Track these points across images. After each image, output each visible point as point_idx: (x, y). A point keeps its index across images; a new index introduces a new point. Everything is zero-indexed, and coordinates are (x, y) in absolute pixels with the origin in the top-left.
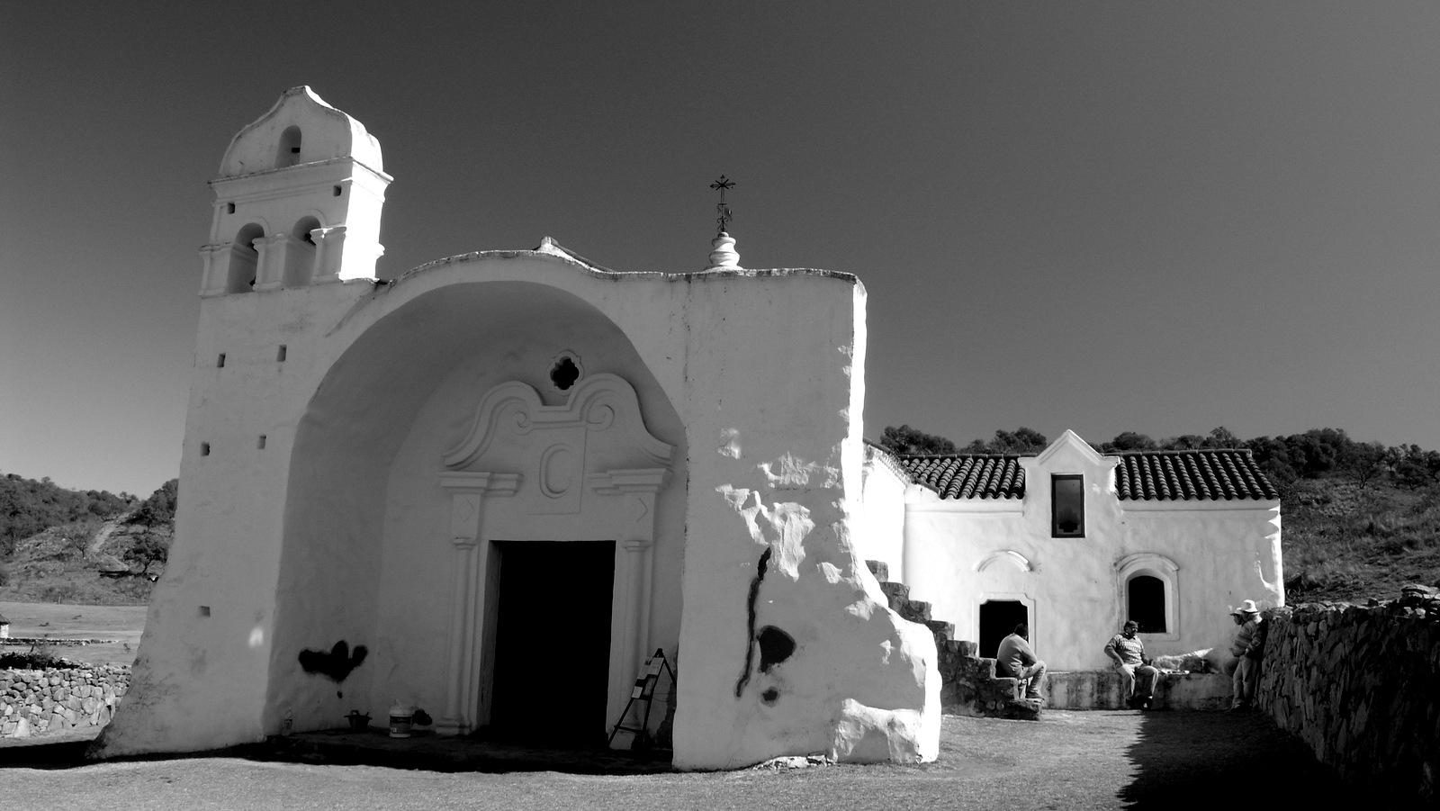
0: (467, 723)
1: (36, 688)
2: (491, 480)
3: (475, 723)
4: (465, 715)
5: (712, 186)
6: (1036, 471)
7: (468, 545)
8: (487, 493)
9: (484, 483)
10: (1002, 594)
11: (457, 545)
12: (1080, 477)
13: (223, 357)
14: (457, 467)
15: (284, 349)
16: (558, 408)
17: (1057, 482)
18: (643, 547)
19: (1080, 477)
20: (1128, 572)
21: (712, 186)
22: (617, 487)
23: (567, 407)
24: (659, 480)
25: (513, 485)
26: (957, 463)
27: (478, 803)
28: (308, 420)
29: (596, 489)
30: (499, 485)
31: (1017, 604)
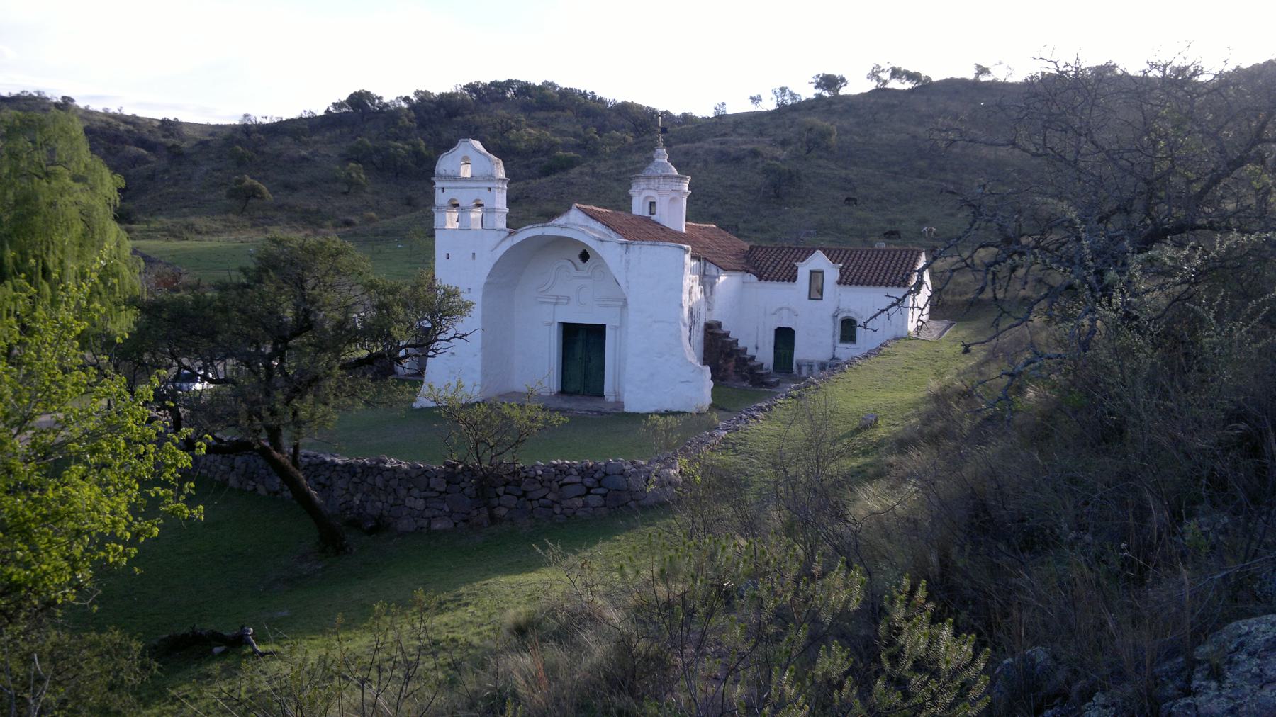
6: (804, 270)
7: (550, 324)
8: (556, 303)
9: (554, 301)
18: (616, 328)
20: (840, 317)
28: (487, 283)
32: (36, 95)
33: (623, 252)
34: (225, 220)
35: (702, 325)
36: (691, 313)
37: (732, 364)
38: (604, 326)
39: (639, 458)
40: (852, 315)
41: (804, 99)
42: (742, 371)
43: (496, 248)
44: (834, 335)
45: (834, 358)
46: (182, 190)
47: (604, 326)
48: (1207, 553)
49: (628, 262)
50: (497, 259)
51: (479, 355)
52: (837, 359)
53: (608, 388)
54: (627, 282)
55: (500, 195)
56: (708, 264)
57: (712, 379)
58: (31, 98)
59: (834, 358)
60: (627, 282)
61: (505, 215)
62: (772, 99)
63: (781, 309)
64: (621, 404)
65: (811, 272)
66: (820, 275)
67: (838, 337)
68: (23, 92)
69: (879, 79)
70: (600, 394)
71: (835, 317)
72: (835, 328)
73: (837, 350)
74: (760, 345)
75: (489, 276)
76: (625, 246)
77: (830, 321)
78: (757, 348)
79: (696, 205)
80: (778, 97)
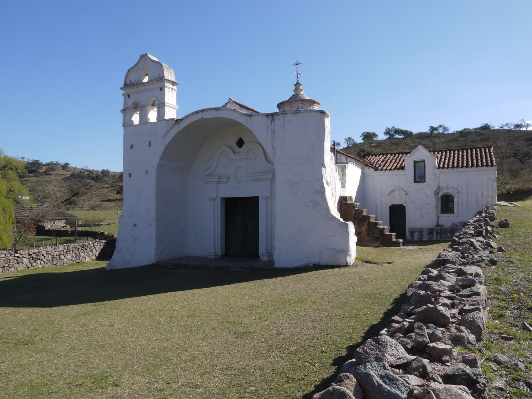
0: (218, 254)
1: (90, 247)
2: (219, 178)
3: (220, 254)
4: (217, 252)
5: (293, 65)
7: (214, 200)
8: (218, 182)
9: (217, 180)
10: (397, 202)
11: (211, 199)
12: (424, 161)
13: (132, 146)
14: (208, 175)
15: (150, 142)
16: (240, 155)
17: (416, 163)
18: (267, 198)
19: (424, 161)
20: (440, 194)
21: (293, 65)
22: (258, 179)
23: (241, 154)
24: (271, 177)
25: (226, 180)
26: (385, 156)
27: (4, 325)
28: (160, 165)
29: (252, 180)
30: (222, 180)
31: (402, 205)
32: (56, 163)
33: (269, 123)
38: (257, 198)
40: (450, 191)
41: (358, 143)
42: (373, 233)
43: (166, 134)
44: (437, 208)
45: (438, 225)
47: (257, 198)
48: (69, 251)
49: (273, 131)
50: (167, 144)
51: (154, 224)
52: (441, 226)
53: (262, 249)
54: (273, 148)
56: (338, 155)
57: (355, 234)
58: (54, 164)
59: (438, 225)
60: (273, 148)
62: (345, 143)
63: (393, 191)
64: (273, 262)
65: (415, 162)
67: (439, 210)
68: (51, 162)
69: (390, 134)
70: (256, 255)
71: (436, 193)
72: (437, 203)
73: (440, 219)
75: (162, 158)
76: (270, 117)
77: (433, 197)
80: (347, 142)
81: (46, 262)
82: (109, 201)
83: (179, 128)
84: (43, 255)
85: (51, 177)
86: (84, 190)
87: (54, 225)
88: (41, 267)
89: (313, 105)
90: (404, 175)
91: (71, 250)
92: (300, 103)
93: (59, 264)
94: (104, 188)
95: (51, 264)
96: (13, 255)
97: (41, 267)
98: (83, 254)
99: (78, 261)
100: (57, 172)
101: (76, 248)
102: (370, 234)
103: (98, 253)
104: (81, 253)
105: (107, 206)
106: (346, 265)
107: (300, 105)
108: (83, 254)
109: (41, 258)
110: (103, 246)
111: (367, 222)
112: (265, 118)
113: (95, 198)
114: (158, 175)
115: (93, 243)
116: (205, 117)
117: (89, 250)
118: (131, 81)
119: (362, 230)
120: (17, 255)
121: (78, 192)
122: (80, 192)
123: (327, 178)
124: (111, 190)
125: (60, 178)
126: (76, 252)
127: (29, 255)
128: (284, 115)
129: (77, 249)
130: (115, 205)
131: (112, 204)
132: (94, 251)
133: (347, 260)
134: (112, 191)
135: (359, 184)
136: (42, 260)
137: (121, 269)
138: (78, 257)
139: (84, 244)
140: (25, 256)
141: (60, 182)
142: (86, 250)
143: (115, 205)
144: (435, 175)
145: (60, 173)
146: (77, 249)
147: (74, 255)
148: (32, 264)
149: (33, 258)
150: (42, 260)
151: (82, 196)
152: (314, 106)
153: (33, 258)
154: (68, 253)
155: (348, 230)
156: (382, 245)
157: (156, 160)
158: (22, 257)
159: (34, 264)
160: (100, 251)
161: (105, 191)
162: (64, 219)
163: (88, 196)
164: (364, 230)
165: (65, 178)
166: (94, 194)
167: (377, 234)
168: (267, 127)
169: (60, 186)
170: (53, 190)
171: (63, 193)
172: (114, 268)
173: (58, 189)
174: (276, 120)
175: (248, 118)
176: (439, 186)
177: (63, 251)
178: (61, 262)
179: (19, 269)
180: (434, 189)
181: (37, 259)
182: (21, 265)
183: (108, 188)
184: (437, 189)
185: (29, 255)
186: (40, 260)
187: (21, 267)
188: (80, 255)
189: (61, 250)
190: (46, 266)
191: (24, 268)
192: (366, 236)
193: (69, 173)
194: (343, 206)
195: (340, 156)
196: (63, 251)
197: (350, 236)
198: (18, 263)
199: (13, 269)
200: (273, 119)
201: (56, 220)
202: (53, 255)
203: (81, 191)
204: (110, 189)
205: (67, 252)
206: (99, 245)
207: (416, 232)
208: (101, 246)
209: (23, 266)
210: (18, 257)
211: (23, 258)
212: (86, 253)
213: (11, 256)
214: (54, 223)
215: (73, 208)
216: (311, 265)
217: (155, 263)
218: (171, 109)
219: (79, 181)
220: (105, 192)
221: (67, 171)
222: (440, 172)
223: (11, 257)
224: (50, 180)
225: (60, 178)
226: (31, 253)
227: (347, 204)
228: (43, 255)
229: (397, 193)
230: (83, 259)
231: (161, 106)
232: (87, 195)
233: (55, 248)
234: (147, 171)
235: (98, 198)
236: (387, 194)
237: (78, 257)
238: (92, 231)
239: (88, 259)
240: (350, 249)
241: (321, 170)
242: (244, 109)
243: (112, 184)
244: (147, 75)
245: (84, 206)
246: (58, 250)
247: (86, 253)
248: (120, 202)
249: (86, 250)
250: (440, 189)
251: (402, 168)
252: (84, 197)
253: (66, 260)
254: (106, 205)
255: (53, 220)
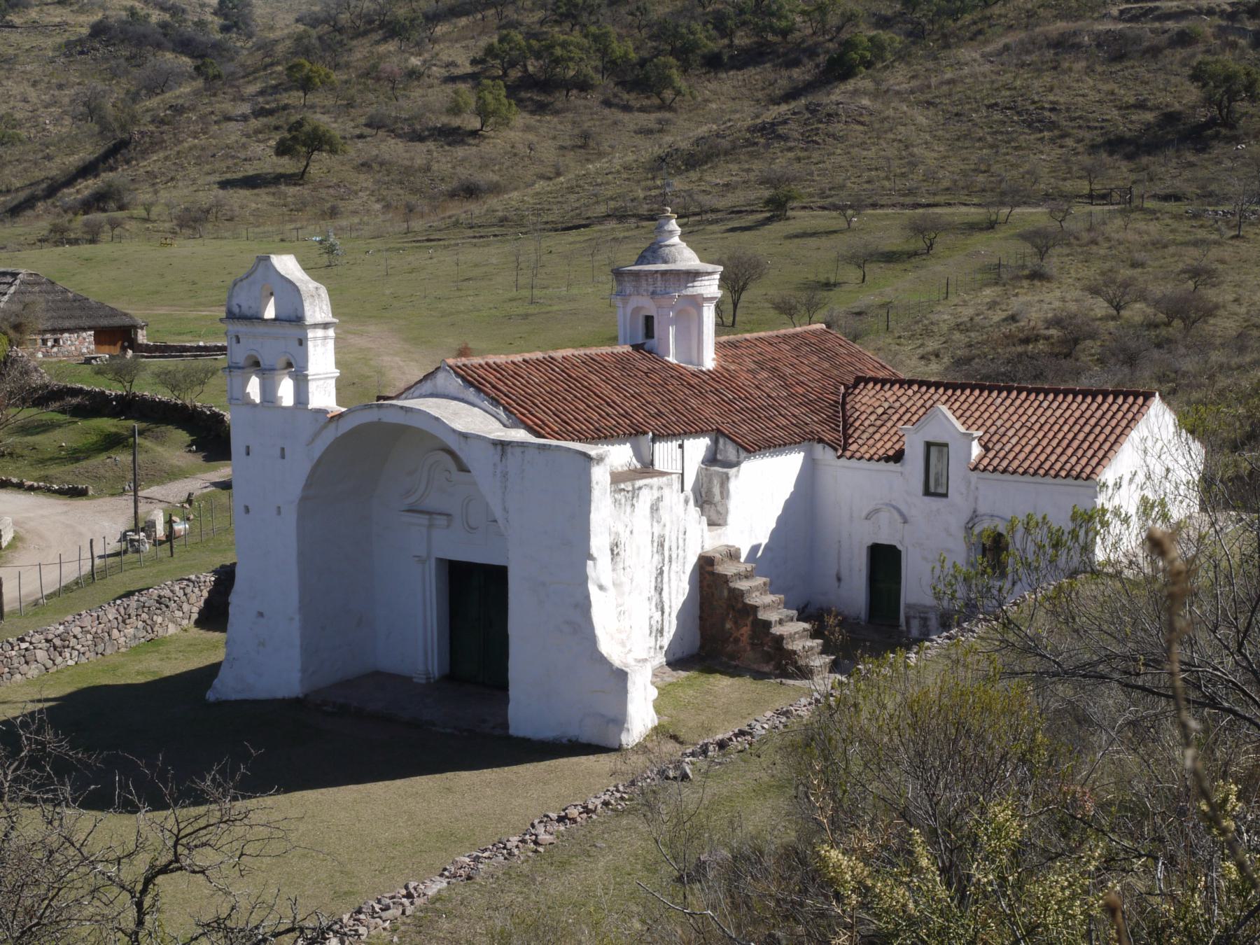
3: (437, 675)
4: (430, 669)
10: (884, 539)
13: (248, 448)
15: (283, 449)
20: (977, 530)
28: (304, 499)
33: (497, 458)
34: (274, 194)
35: (692, 560)
36: (662, 545)
37: (746, 631)
39: (459, 854)
42: (762, 644)
43: (313, 440)
46: (214, 142)
49: (505, 475)
51: (297, 617)
55: (320, 349)
61: (333, 382)
66: (945, 449)
71: (969, 528)
74: (844, 574)
75: (308, 486)
78: (839, 579)
79: (1061, 147)
81: (82, 650)
82: (251, 182)
83: (337, 429)
84: (75, 637)
85: (14, 37)
86: (152, 128)
87: (55, 349)
88: (73, 663)
89: (694, 281)
90: (902, 473)
91: (133, 613)
92: (659, 278)
93: (108, 651)
94: (229, 119)
95: (93, 654)
96: (16, 648)
97: (73, 663)
98: (159, 619)
99: (149, 637)
100: (33, 14)
101: (144, 607)
102: (756, 645)
103: (195, 610)
104: (155, 617)
105: (242, 207)
106: (619, 749)
107: (659, 284)
108: (159, 619)
109: (71, 645)
110: (209, 592)
111: (751, 618)
112: (491, 448)
113: (193, 171)
114: (301, 517)
115: (184, 589)
116: (385, 420)
117: (172, 605)
118: (240, 306)
119: (742, 635)
120: (24, 645)
121: (125, 136)
122: (137, 137)
123: (598, 579)
124: (257, 132)
125: (50, 42)
126: (144, 616)
127: (47, 641)
128: (522, 449)
129: (146, 610)
130: (272, 204)
131: (259, 199)
132: (186, 607)
133: (620, 740)
134: (260, 136)
135: (792, 494)
136: (73, 648)
137: (236, 701)
138: (149, 628)
139: (162, 594)
140: (40, 646)
141: (52, 61)
142: (167, 607)
143: (272, 204)
144: (969, 482)
145: (47, 20)
146: (146, 610)
147: (140, 624)
148: (53, 661)
149: (55, 648)
150: (73, 648)
151: (144, 153)
152: (696, 284)
153: (55, 648)
154: (128, 621)
155: (626, 684)
156: (777, 672)
157: (294, 486)
158: (35, 648)
159: (59, 660)
160: (202, 604)
161: (233, 132)
162: (90, 329)
163: (166, 158)
164: (746, 636)
165: (69, 44)
166: (191, 149)
167: (770, 647)
168: (495, 465)
169: (54, 81)
170: (26, 101)
171: (65, 113)
172: (224, 698)
173: (46, 98)
174: (509, 455)
175: (462, 438)
176: (975, 512)
177: (117, 619)
178: (113, 644)
179: (29, 676)
180: (965, 516)
181: (64, 647)
182: (33, 667)
183: (245, 118)
184: (972, 519)
185: (47, 641)
186: (69, 650)
187: (33, 671)
188: (155, 623)
189: (111, 617)
190: (83, 660)
191: (40, 671)
192: (748, 648)
193: (82, 19)
194: (707, 575)
195: (725, 444)
196: (117, 619)
197: (629, 696)
198: (27, 663)
199: (18, 676)
200: (503, 453)
201: (63, 331)
202: (96, 633)
203: (141, 133)
204: (255, 123)
205: (124, 621)
206: (196, 590)
207: (915, 617)
208: (201, 591)
209: (37, 668)
210: (26, 649)
211: (37, 651)
212: (168, 613)
213: (13, 650)
214: (56, 341)
215: (114, 224)
216: (564, 741)
217: (301, 696)
218: (322, 382)
219: (127, 59)
220: (233, 138)
221: (75, 7)
222: (979, 478)
223: (14, 653)
224: (11, 51)
225: (49, 43)
226: (50, 637)
227: (713, 574)
228: (75, 637)
229: (884, 516)
230: (160, 631)
231: (298, 371)
232: (162, 155)
233: (98, 616)
234: (279, 508)
235: (207, 168)
236: (864, 514)
237: (149, 628)
238: (184, 407)
239: (172, 629)
240: (629, 719)
241: (585, 566)
242: (472, 389)
243: (261, 99)
244: (272, 294)
245: (155, 210)
246: (104, 619)
247: (168, 613)
248: (292, 190)
249: (167, 607)
250: (976, 520)
251: (898, 457)
252: (153, 162)
253: (124, 639)
254: (236, 207)
255: (54, 331)
